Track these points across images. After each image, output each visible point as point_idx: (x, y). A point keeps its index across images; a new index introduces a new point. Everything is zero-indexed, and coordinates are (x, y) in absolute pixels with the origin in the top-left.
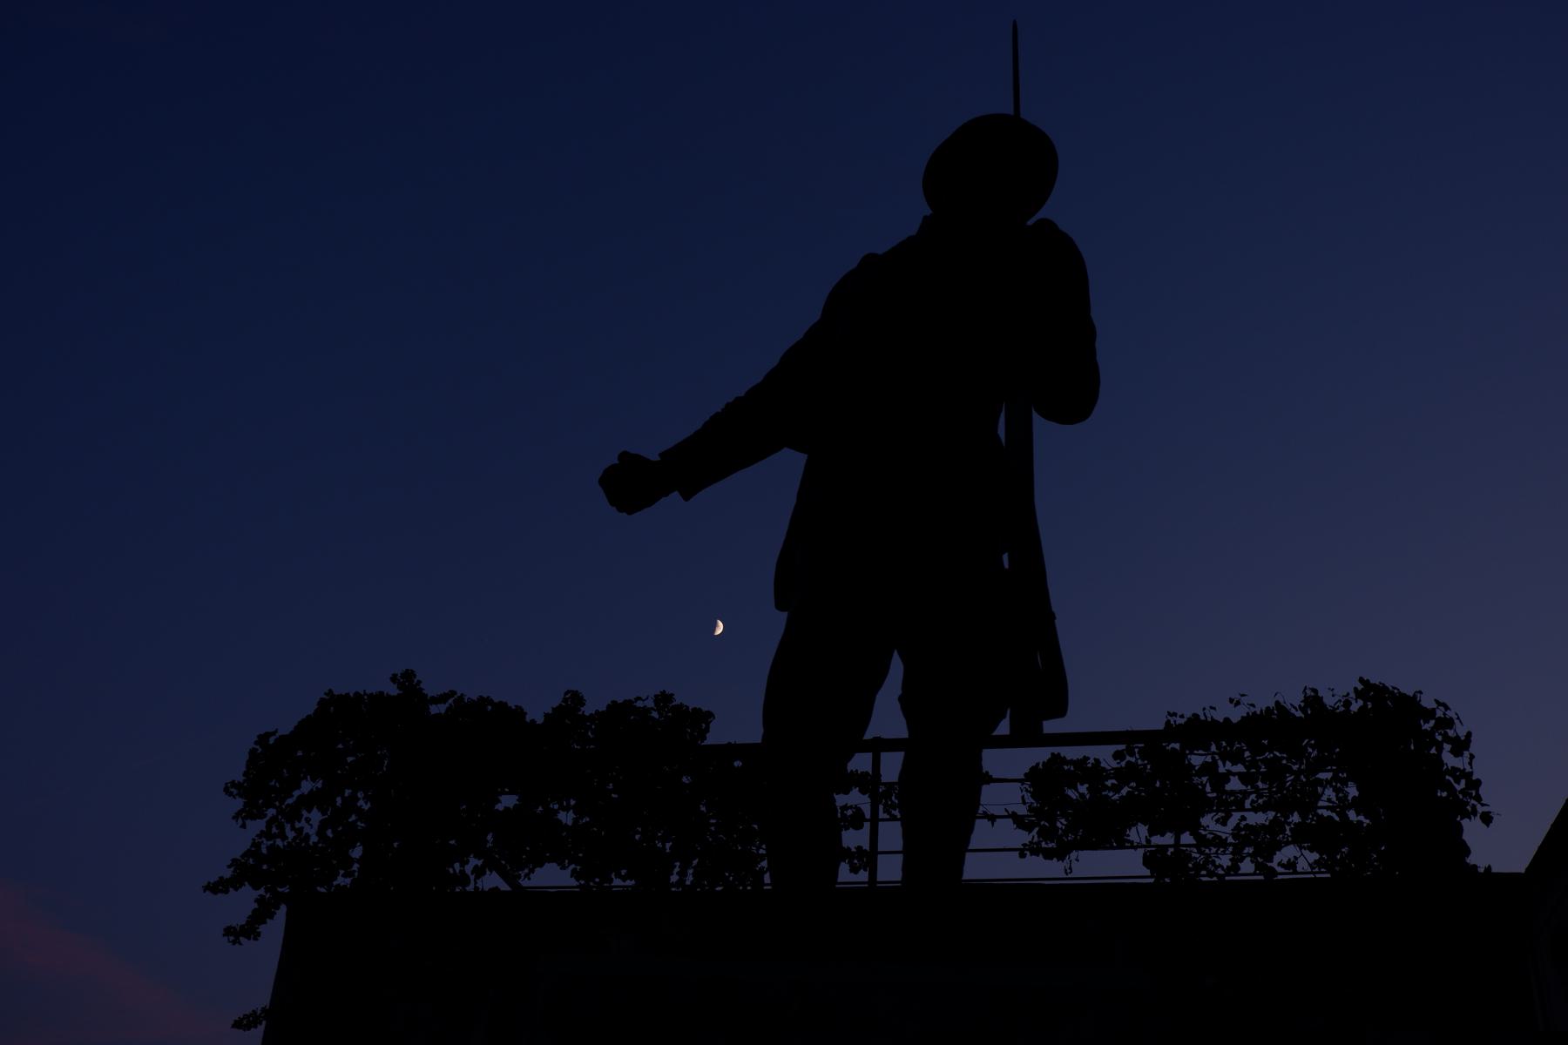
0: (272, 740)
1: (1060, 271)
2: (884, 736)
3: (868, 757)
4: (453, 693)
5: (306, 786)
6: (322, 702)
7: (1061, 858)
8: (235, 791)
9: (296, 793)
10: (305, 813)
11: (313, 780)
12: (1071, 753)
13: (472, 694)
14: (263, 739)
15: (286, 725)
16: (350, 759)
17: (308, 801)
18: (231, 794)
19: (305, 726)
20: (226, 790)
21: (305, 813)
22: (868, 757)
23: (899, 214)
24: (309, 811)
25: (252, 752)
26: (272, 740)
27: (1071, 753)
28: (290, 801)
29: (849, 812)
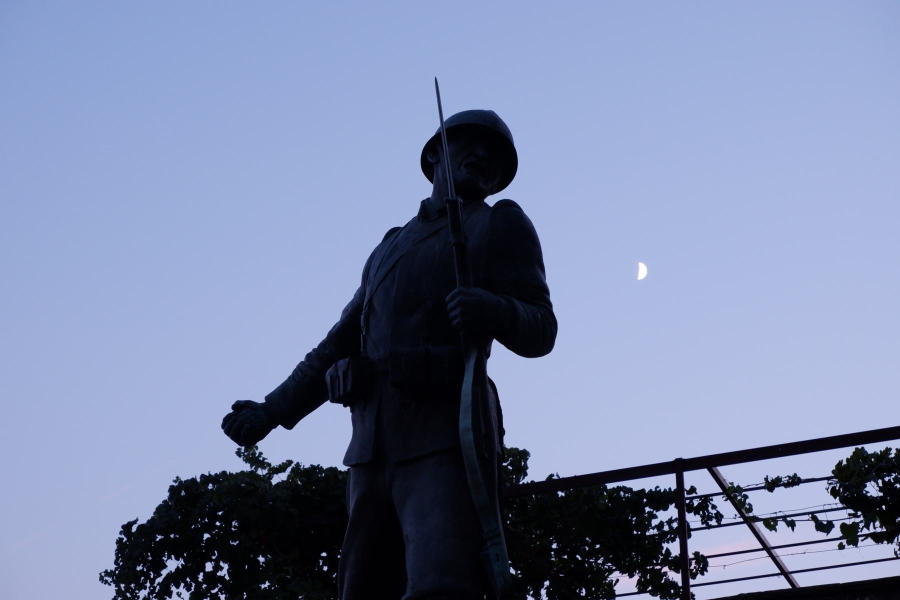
0: (134, 528)
1: (517, 240)
2: (685, 457)
3: (673, 477)
4: (290, 462)
5: (172, 565)
6: (172, 489)
7: (890, 541)
8: (109, 579)
9: (164, 572)
10: (173, 588)
11: (177, 559)
12: (873, 448)
13: (306, 464)
14: (127, 528)
15: (145, 515)
16: (206, 536)
17: (175, 578)
18: (106, 582)
19: (161, 510)
20: (101, 579)
21: (173, 588)
22: (673, 477)
23: (407, 194)
24: (178, 587)
25: (119, 541)
26: (134, 528)
27: (873, 448)
28: (159, 580)
29: (675, 525)
